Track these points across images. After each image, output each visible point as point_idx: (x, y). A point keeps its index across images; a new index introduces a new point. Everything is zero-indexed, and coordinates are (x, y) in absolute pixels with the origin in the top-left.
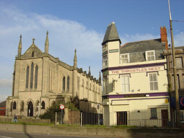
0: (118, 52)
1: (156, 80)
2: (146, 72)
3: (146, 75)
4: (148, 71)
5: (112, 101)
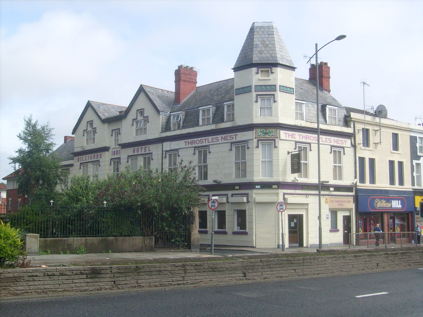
0: (294, 94)
1: (340, 162)
2: (330, 147)
3: (330, 151)
4: (298, 139)
5: (284, 194)
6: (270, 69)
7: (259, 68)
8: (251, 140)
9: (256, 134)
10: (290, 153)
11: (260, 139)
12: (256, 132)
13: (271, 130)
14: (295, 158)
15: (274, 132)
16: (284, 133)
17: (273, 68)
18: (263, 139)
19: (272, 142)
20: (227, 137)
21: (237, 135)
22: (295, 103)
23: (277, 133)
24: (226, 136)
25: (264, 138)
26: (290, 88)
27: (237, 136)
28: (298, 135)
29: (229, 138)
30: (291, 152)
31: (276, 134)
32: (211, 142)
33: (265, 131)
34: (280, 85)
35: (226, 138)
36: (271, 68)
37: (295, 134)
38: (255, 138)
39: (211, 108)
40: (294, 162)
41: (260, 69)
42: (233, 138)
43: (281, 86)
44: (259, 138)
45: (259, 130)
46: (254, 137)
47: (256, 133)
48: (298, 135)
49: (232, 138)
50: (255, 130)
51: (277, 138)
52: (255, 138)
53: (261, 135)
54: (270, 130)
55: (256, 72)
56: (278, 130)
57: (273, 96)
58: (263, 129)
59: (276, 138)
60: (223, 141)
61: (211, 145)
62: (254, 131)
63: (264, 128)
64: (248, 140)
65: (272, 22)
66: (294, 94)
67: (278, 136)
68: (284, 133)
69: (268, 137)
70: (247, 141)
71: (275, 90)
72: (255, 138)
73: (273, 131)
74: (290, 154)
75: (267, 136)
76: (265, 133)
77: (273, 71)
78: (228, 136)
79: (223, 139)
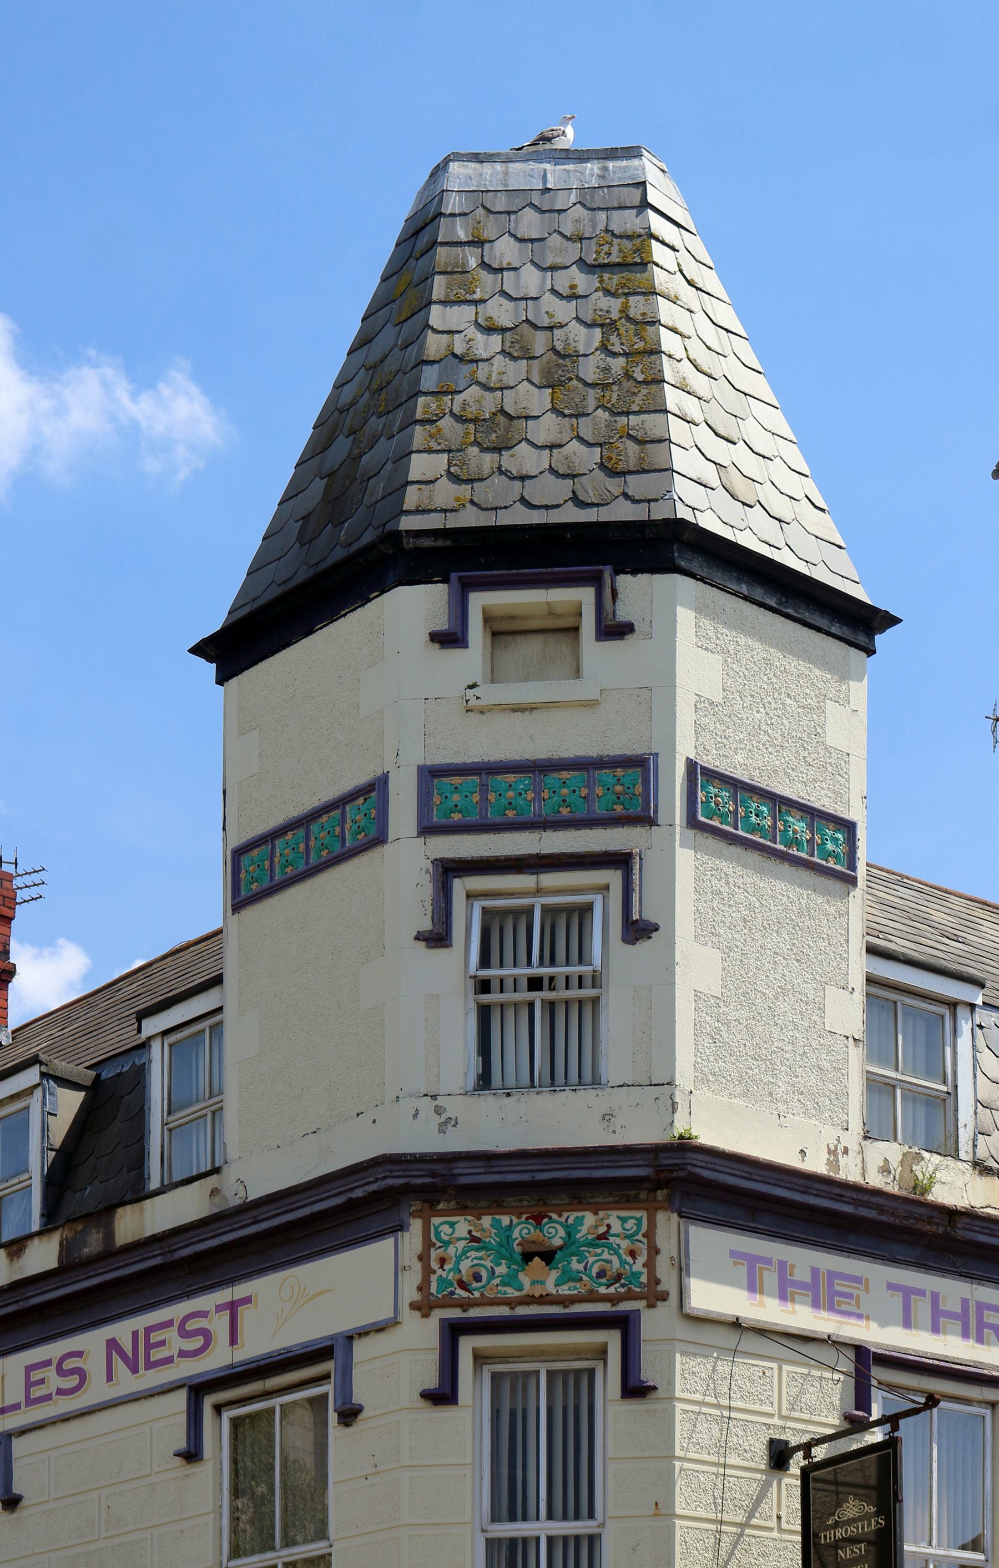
6: (585, 596)
7: (467, 586)
8: (379, 1328)
9: (427, 1271)
10: (800, 1454)
11: (475, 1313)
12: (428, 1245)
13: (589, 1219)
14: (839, 1505)
15: (625, 1244)
16: (733, 1254)
17: (624, 581)
18: (504, 1311)
19: (601, 1353)
20: (155, 1337)
21: (247, 1300)
22: (857, 981)
23: (654, 1251)
24: (148, 1330)
25: (511, 1303)
26: (813, 814)
27: (244, 1313)
28: (891, 1286)
29: (176, 1343)
30: (807, 1448)
31: (641, 1260)
32: (16, 1407)
33: (522, 1230)
34: (691, 766)
35: (149, 1346)
36: (595, 580)
37: (857, 1280)
38: (414, 1306)
39: (38, 1093)
40: (840, 1533)
41: (479, 601)
42: (207, 1335)
43: (712, 775)
44: (465, 1305)
45: (463, 1226)
46: (410, 1293)
47: (423, 1258)
48: (891, 1286)
49: (198, 1342)
50: (416, 1225)
51: (655, 1297)
52: (414, 1306)
53: (477, 1278)
54: (579, 1221)
55: (442, 624)
56: (661, 1217)
57: (613, 877)
58: (505, 1220)
59: (639, 1305)
60: (127, 1382)
61: (23, 1432)
62: (412, 1238)
63: (511, 1201)
64: (350, 1338)
65: (632, 152)
66: (853, 881)
67: (668, 1282)
68: (733, 1254)
69: (565, 1290)
70: (338, 1352)
71: (636, 810)
72: (424, 1307)
73: (616, 1227)
74: (797, 1462)
75: (551, 1283)
76: (527, 1257)
77: (624, 612)
78: (168, 1324)
79: (120, 1367)
